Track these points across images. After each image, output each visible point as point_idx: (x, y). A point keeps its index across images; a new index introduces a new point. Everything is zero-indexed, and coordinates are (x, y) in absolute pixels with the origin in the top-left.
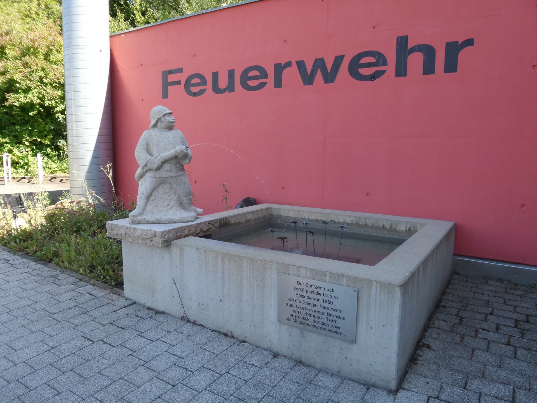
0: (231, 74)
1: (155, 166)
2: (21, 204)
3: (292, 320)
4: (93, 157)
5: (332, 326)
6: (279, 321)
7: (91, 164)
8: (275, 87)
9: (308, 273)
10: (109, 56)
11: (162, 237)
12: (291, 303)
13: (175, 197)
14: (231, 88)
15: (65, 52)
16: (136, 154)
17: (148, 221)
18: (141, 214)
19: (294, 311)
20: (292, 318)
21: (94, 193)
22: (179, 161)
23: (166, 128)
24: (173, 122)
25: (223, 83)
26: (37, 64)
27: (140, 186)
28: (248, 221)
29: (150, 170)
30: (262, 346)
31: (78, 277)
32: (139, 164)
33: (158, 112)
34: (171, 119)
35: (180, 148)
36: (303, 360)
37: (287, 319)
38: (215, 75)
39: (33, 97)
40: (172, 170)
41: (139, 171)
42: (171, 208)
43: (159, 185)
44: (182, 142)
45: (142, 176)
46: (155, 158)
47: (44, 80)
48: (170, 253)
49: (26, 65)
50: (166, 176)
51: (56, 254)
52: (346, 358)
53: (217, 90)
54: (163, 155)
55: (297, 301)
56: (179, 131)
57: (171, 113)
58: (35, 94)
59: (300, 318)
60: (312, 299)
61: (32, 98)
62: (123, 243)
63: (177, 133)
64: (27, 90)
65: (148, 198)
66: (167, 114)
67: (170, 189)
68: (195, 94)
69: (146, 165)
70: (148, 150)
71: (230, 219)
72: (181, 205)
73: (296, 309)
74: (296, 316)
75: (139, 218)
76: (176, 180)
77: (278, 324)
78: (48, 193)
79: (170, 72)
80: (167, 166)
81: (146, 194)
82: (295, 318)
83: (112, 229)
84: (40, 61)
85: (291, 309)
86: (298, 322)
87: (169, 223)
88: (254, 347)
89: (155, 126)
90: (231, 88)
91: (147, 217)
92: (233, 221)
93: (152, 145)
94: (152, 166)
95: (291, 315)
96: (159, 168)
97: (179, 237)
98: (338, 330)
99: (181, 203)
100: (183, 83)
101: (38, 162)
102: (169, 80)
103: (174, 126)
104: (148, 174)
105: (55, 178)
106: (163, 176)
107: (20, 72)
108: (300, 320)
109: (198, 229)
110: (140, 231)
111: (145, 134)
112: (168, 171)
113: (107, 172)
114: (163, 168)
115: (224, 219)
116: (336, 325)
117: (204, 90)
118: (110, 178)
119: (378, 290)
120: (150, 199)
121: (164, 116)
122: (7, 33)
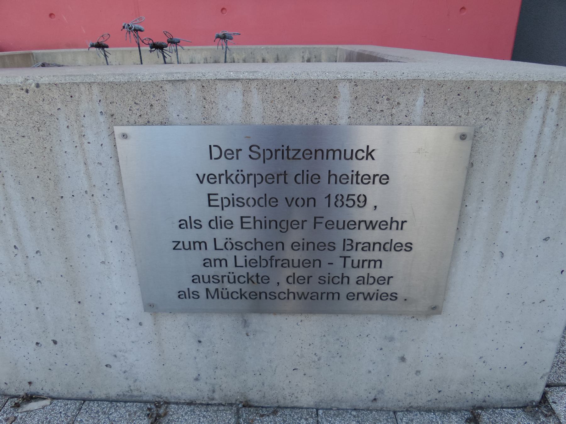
3: (203, 294)
5: (361, 281)
6: (151, 307)
9: (255, 98)
12: (190, 235)
19: (207, 263)
20: (201, 288)
30: (99, 393)
36: (254, 396)
37: (182, 295)
52: (403, 359)
55: (217, 223)
59: (236, 280)
60: (282, 203)
73: (212, 254)
74: (216, 279)
77: (147, 319)
82: (212, 287)
85: (197, 256)
86: (230, 296)
88: (73, 406)
95: (196, 279)
98: (384, 289)
108: (232, 288)
116: (376, 273)
119: (552, 117)
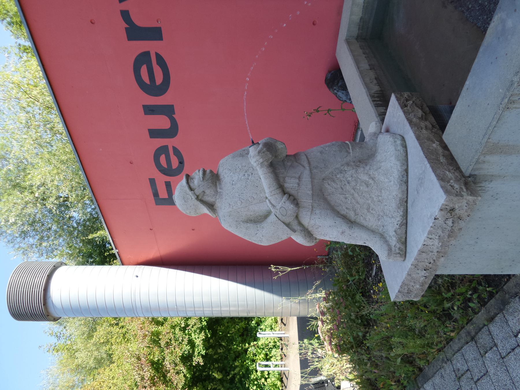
0: (149, 110)
1: (290, 207)
2: (323, 383)
4: (263, 289)
7: (271, 291)
8: (161, 38)
10: (459, 162)
11: (459, 195)
13: (350, 172)
14: (168, 110)
15: (140, 315)
16: (265, 243)
17: (401, 225)
18: (382, 237)
21: (310, 291)
22: (278, 164)
23: (216, 186)
24: (204, 172)
25: (162, 122)
26: (167, 333)
27: (327, 238)
28: (372, 67)
29: (297, 217)
31: (463, 341)
32: (285, 237)
33: (185, 199)
34: (197, 176)
35: (254, 157)
38: (154, 133)
39: (199, 339)
40: (297, 176)
41: (300, 239)
42: (373, 179)
43: (326, 200)
44: (242, 156)
45: (308, 233)
46: (273, 206)
47: (183, 326)
48: (491, 178)
49: (168, 344)
50: (310, 186)
51: (408, 360)
53: (172, 132)
54: (267, 191)
56: (221, 162)
57: (188, 177)
58: (197, 337)
61: (200, 339)
62: (438, 273)
63: (227, 168)
64: (191, 343)
65: (351, 223)
66: (188, 183)
67: (334, 181)
68: (181, 163)
69: (288, 225)
70: (259, 220)
71: (373, 91)
72: (367, 158)
75: (393, 242)
76: (316, 167)
78: (306, 341)
79: (156, 194)
80: (290, 184)
81: (344, 227)
83: (409, 292)
84: (164, 329)
87: (407, 182)
89: (211, 206)
90: (168, 110)
91: (391, 227)
92: (376, 88)
93: (246, 201)
94: (289, 212)
96: (295, 200)
97: (451, 160)
99: (360, 162)
100: (168, 179)
101: (265, 336)
102: (166, 196)
103: (211, 172)
104: (306, 220)
105: (282, 320)
106: (310, 193)
107: (174, 349)
109: (423, 124)
110: (430, 242)
111: (225, 226)
112: (300, 182)
113: (282, 272)
114: (293, 192)
115: (373, 101)
117: (174, 149)
118: (290, 269)
120: (353, 220)
121: (191, 189)
122: (139, 359)
